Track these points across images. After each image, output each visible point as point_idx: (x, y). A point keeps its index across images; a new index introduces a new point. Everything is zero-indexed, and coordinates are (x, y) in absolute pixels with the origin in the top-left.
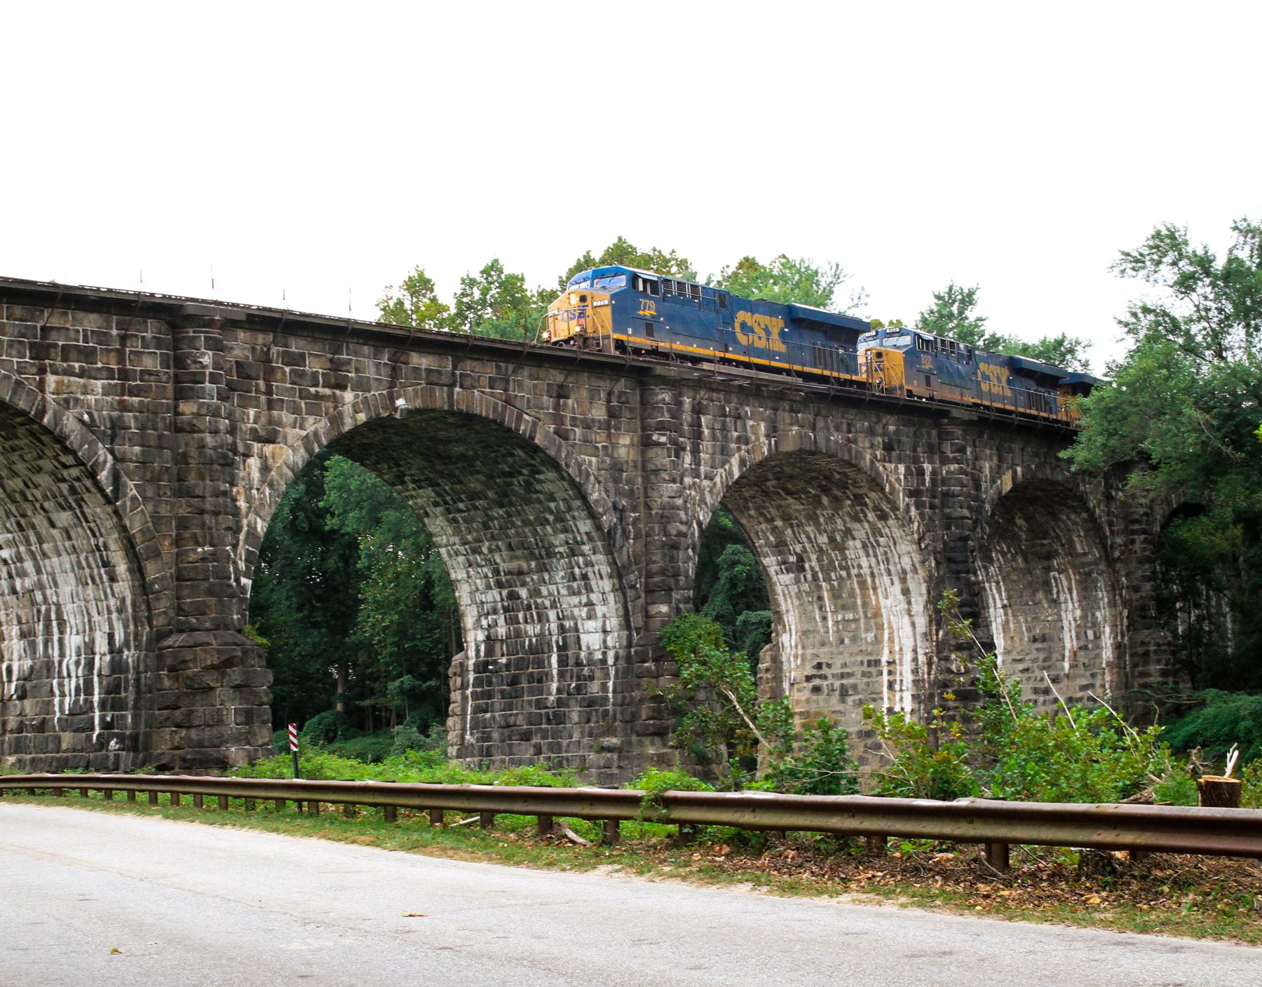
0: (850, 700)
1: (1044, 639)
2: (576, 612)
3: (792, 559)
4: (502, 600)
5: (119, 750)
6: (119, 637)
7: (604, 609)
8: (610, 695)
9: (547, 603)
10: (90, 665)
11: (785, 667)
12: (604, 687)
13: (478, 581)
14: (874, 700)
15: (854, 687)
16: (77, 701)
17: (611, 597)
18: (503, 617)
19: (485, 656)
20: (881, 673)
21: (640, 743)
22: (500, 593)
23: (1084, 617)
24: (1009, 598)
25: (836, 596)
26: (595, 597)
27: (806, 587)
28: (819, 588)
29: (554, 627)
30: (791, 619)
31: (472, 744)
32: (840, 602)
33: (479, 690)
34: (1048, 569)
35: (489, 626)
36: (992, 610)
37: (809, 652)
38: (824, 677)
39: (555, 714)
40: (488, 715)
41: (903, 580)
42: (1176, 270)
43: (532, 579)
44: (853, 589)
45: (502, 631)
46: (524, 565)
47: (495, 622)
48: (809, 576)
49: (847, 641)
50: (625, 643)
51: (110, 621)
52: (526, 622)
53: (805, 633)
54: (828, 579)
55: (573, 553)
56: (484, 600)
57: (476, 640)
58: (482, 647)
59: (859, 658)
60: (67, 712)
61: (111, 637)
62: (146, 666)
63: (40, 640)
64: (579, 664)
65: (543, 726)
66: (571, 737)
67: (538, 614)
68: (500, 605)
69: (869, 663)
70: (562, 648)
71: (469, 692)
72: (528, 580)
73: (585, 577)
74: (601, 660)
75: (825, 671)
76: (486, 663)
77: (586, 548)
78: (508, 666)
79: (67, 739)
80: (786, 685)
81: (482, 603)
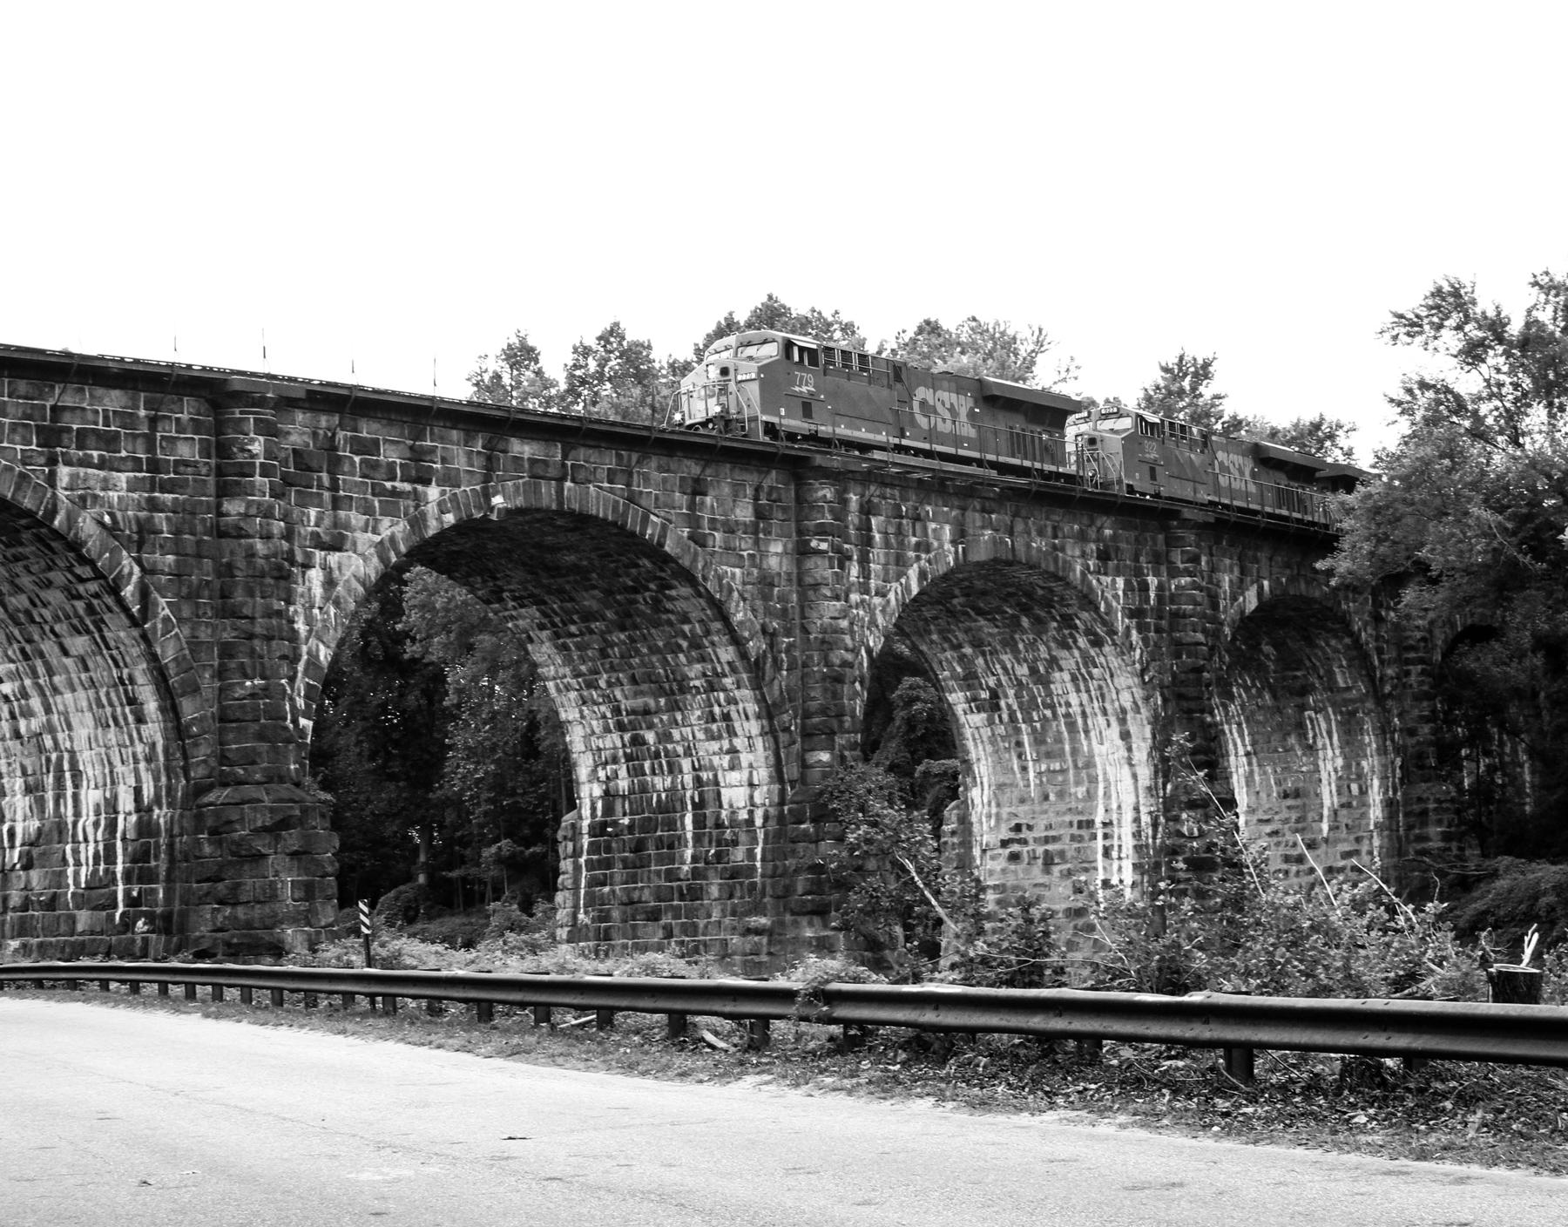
0: (1056, 870)
1: (1297, 794)
3: (985, 695)
4: (624, 746)
5: (148, 932)
6: (148, 791)
7: (751, 757)
8: (758, 864)
9: (680, 750)
10: (112, 826)
11: (976, 828)
12: (750, 854)
13: (594, 723)
15: (1062, 854)
16: (95, 871)
17: (759, 743)
18: (624, 766)
19: (603, 816)
20: (1094, 837)
21: (796, 924)
22: (622, 738)
23: (1347, 767)
24: (1253, 744)
25: (1038, 740)
27: (1001, 730)
28: (1018, 731)
29: (688, 779)
30: (983, 770)
31: (586, 925)
32: (1043, 748)
33: (595, 857)
34: (1302, 708)
35: (608, 778)
36: (1232, 758)
37: (1005, 811)
38: (1024, 842)
39: (689, 888)
40: (607, 889)
41: (1122, 721)
42: (1461, 335)
43: (661, 720)
44: (1059, 732)
45: (623, 784)
46: (652, 703)
48: (1005, 717)
49: (1052, 797)
50: (776, 800)
52: (653, 773)
53: (1001, 787)
54: (1028, 720)
56: (601, 746)
57: (591, 795)
58: (599, 805)
59: (1067, 818)
60: (83, 886)
61: (138, 792)
62: (182, 828)
63: (50, 796)
64: (719, 825)
65: (675, 903)
66: (709, 916)
67: (669, 763)
68: (621, 752)
69: (1080, 825)
70: (699, 806)
71: (582, 860)
72: (656, 720)
73: (726, 717)
74: (746, 820)
75: (1025, 834)
76: (604, 825)
77: (728, 681)
78: (631, 828)
79: (84, 918)
80: (976, 852)
81: (599, 749)
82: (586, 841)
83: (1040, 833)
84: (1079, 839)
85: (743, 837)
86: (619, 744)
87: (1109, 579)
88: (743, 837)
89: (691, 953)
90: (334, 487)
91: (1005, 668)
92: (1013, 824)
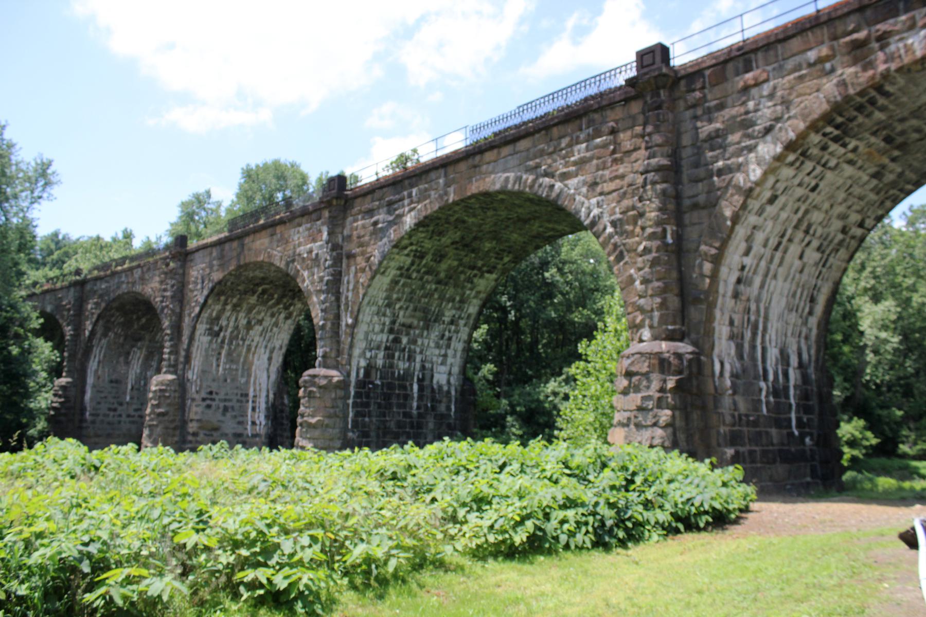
0: (229, 415)
1: (117, 382)
2: (435, 359)
3: (216, 328)
4: (387, 341)
6: (805, 356)
7: (453, 360)
9: (418, 350)
12: (449, 408)
14: (242, 416)
15: (233, 408)
20: (248, 401)
23: (141, 373)
24: (105, 356)
25: (229, 354)
27: (214, 346)
28: (222, 347)
29: (418, 366)
30: (197, 363)
33: (359, 400)
34: (133, 346)
38: (213, 400)
39: (417, 423)
40: (367, 419)
41: (272, 352)
44: (241, 352)
47: (376, 356)
48: (219, 340)
49: (229, 381)
51: (799, 343)
52: (399, 359)
54: (231, 343)
58: (362, 371)
59: (235, 391)
65: (407, 430)
68: (384, 345)
69: (242, 395)
70: (420, 381)
71: (350, 401)
72: (412, 332)
73: (450, 339)
75: (214, 396)
77: (462, 322)
81: (372, 340)
83: (222, 396)
84: (241, 401)
85: (444, 400)
86: (385, 340)
88: (444, 400)
91: (236, 319)
92: (209, 390)
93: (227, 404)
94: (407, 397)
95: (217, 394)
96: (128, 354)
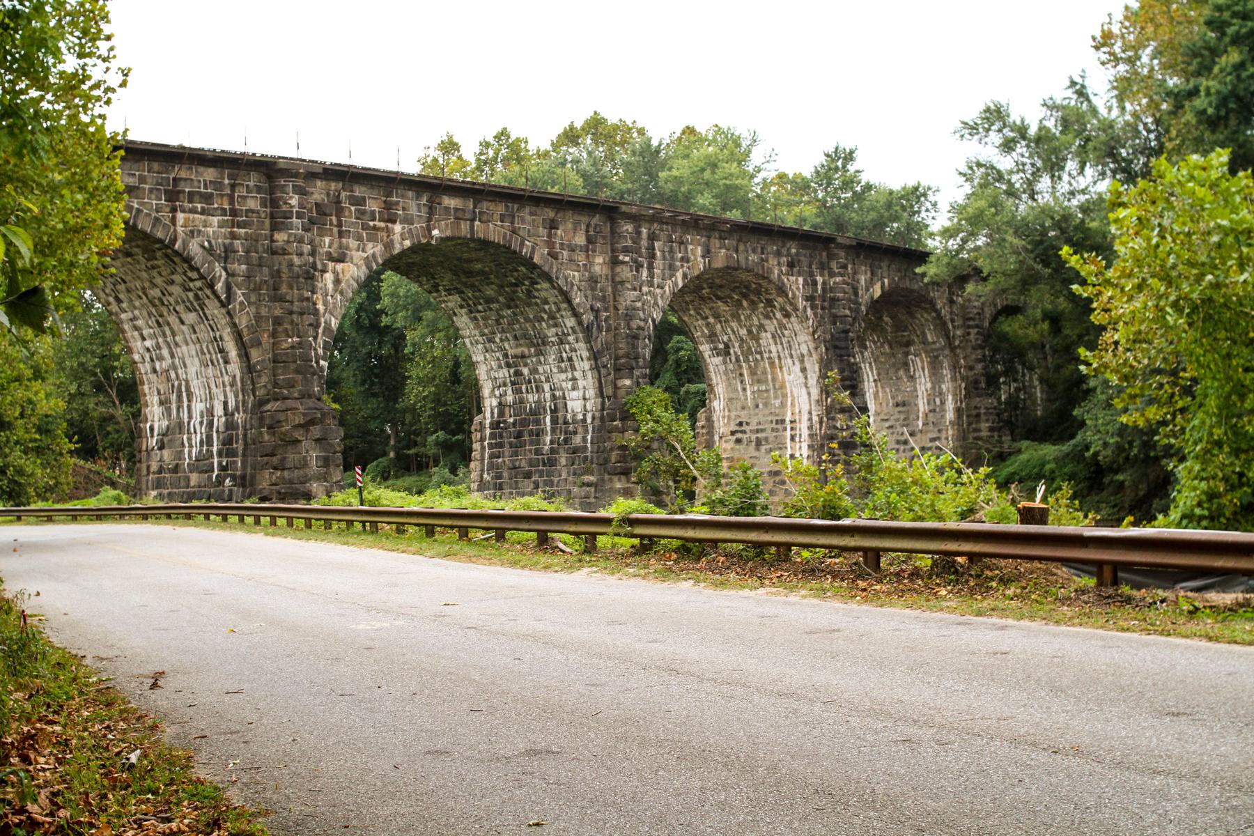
0: (763, 448)
2: (564, 384)
3: (721, 346)
6: (232, 404)
7: (584, 382)
8: (589, 445)
9: (543, 378)
10: (210, 424)
11: (716, 424)
12: (584, 439)
15: (766, 439)
17: (589, 374)
20: (785, 429)
23: (933, 388)
24: (879, 374)
25: (753, 373)
26: (578, 374)
27: (731, 366)
28: (741, 367)
29: (548, 396)
34: (907, 354)
37: (733, 414)
38: (744, 432)
39: (548, 459)
40: (500, 460)
41: (802, 361)
42: (1001, 135)
44: (765, 368)
45: (510, 398)
46: (526, 351)
48: (733, 359)
49: (761, 406)
50: (599, 407)
52: (528, 392)
53: (731, 400)
55: (561, 342)
58: (496, 411)
59: (770, 418)
61: (225, 404)
62: (251, 425)
63: (174, 406)
64: (566, 422)
67: (536, 386)
68: (508, 380)
69: (777, 422)
71: (486, 443)
72: (529, 361)
73: (570, 359)
75: (745, 427)
76: (499, 423)
77: (571, 338)
78: (514, 424)
79: (194, 478)
80: (716, 438)
81: (496, 378)
82: (488, 432)
84: (777, 430)
85: (580, 430)
86: (507, 375)
87: (794, 278)
88: (580, 430)
89: (549, 497)
90: (340, 225)
93: (759, 435)
94: (539, 433)
95: (748, 424)
96: (906, 364)
